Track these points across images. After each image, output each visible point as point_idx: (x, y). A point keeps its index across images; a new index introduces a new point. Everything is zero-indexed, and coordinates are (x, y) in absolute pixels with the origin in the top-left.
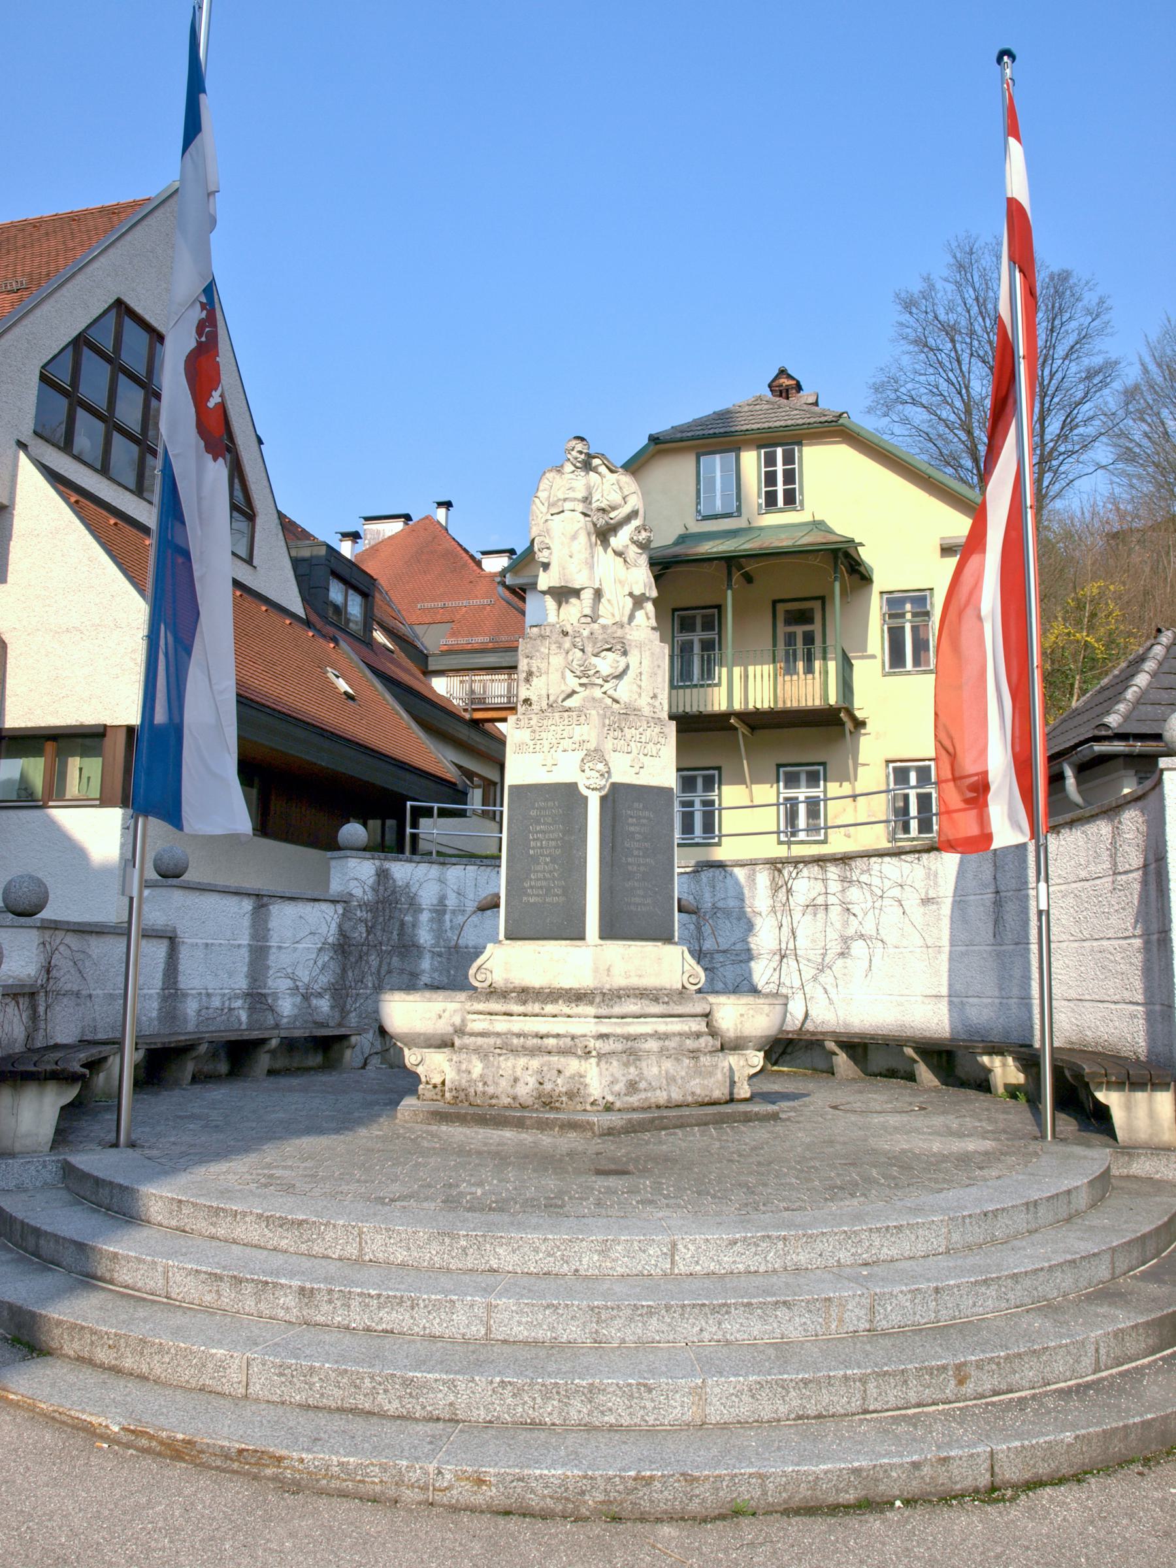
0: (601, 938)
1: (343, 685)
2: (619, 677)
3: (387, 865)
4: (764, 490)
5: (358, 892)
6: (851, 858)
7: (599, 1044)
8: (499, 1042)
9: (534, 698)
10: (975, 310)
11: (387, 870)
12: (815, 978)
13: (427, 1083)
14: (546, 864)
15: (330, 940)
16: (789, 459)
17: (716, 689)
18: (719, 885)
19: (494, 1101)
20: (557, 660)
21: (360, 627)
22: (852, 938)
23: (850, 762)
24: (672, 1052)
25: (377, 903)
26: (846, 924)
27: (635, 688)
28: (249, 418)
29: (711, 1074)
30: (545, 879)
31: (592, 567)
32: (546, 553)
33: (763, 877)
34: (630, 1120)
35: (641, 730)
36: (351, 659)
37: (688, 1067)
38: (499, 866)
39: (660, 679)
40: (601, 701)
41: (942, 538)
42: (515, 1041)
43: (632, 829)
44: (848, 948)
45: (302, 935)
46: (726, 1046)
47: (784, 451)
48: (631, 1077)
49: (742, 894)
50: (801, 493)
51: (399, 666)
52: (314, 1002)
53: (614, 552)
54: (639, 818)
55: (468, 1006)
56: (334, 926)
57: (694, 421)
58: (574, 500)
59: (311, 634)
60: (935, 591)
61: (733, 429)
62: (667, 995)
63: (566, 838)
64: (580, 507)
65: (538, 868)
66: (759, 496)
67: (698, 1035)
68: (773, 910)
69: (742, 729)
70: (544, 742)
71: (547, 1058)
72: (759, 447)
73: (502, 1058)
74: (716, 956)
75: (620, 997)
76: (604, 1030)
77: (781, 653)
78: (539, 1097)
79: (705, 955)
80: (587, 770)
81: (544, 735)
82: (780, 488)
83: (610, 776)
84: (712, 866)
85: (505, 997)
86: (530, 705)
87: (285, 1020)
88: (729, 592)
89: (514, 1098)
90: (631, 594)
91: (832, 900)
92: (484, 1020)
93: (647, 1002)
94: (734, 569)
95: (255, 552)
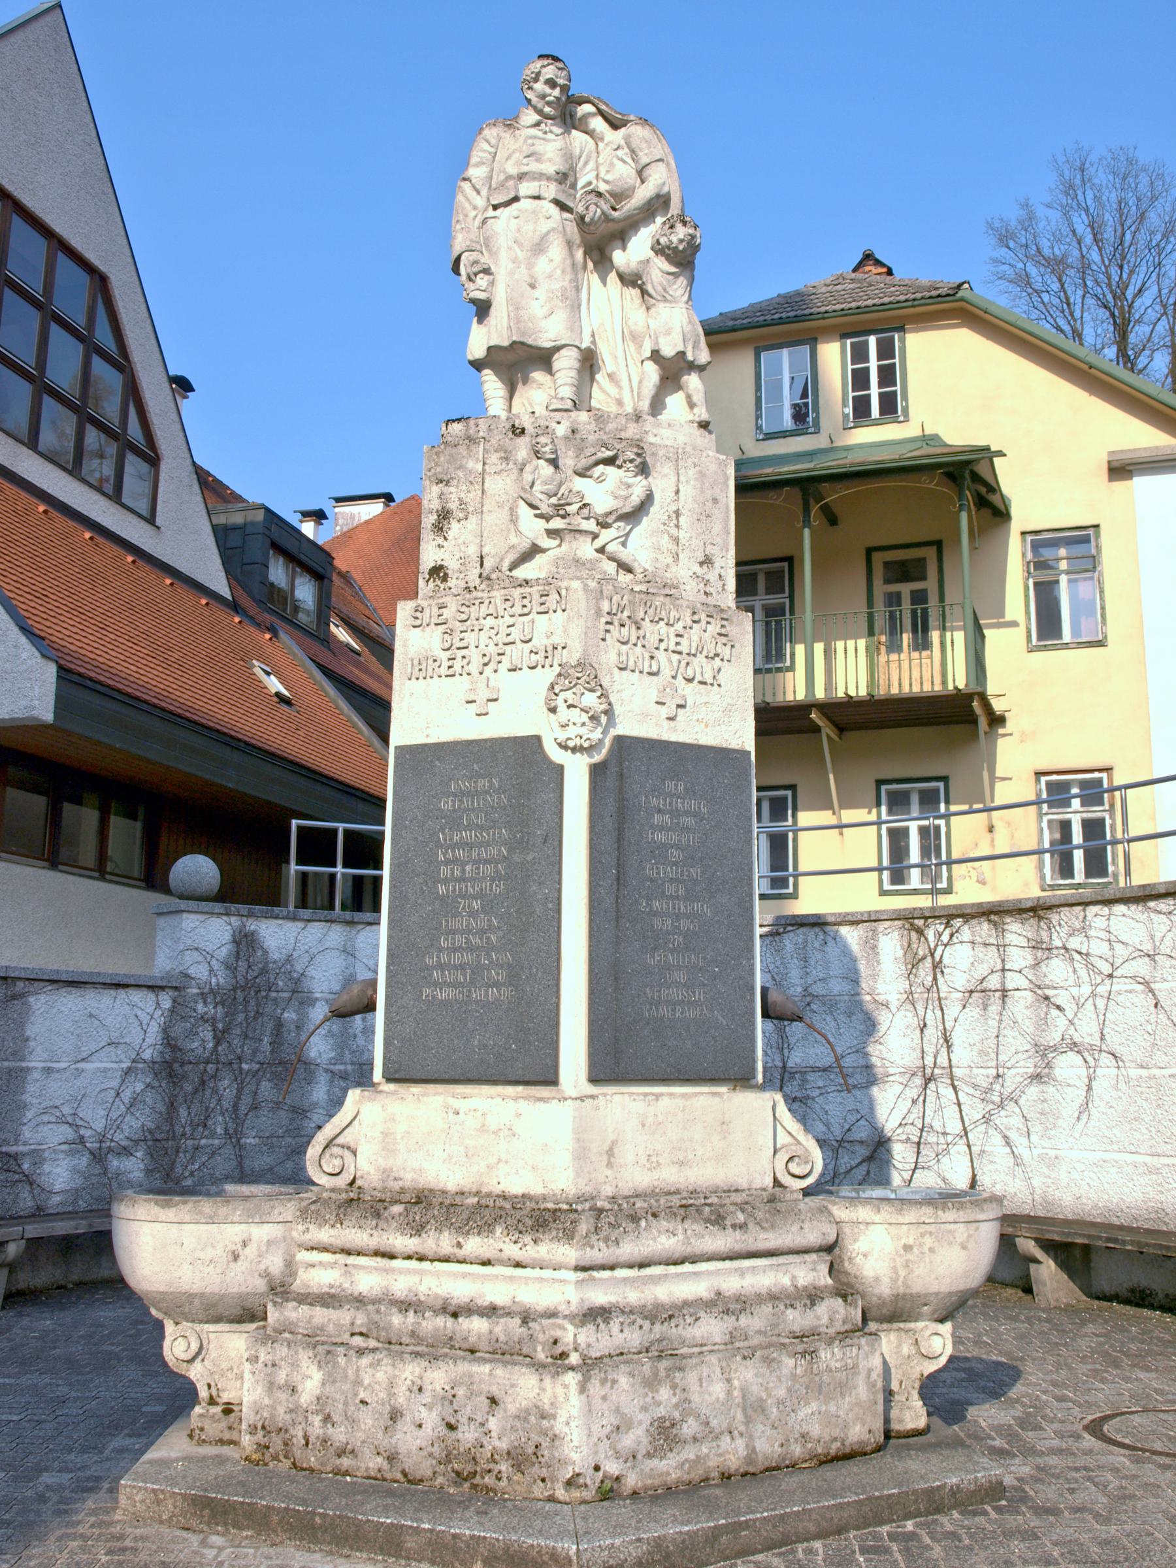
0: (594, 1080)
1: (274, 685)
2: (634, 515)
3: (252, 925)
4: (851, 395)
5: (200, 972)
6: (1050, 908)
7: (585, 1335)
8: (361, 1319)
9: (452, 565)
10: (1089, 239)
11: (253, 933)
12: (987, 1119)
13: (212, 1401)
14: (473, 914)
15: (147, 1055)
16: (886, 350)
17: (789, 675)
18: (815, 957)
19: (346, 1462)
20: (501, 486)
21: (314, 617)
22: (1055, 1048)
23: (985, 774)
24: (755, 1341)
25: (234, 989)
26: (1043, 1023)
27: (665, 540)
28: (150, 328)
29: (843, 1388)
30: (471, 949)
31: (576, 307)
32: (482, 281)
33: (891, 943)
34: (658, 1543)
35: (679, 627)
36: (294, 655)
37: (794, 1377)
38: (379, 924)
39: (717, 527)
40: (592, 565)
41: (1111, 453)
42: (396, 1319)
43: (661, 837)
44: (1048, 1065)
45: (93, 1047)
46: (874, 1312)
47: (878, 341)
48: (661, 1411)
49: (856, 971)
50: (905, 397)
51: (367, 671)
52: (115, 1163)
53: (621, 277)
54: (675, 814)
55: (298, 1232)
56: (154, 1031)
57: (751, 306)
58: (540, 176)
59: (237, 619)
60: (1103, 531)
61: (807, 312)
62: (742, 1207)
63: (516, 858)
64: (551, 190)
65: (455, 924)
66: (845, 404)
67: (812, 1297)
68: (910, 999)
69: (828, 730)
70: (473, 653)
71: (464, 1367)
72: (844, 336)
73: (364, 1361)
74: (811, 1077)
75: (635, 1218)
76: (600, 1297)
77: (880, 622)
78: (448, 1459)
79: (792, 1075)
80: (562, 707)
81: (470, 638)
82: (874, 391)
83: (611, 722)
84: (802, 925)
85: (377, 1215)
86: (445, 579)
87: (56, 1199)
88: (807, 532)
89: (391, 1458)
90: (656, 356)
91: (1013, 981)
92: (333, 1265)
93: (698, 1227)
94: (812, 501)
95: (159, 508)
